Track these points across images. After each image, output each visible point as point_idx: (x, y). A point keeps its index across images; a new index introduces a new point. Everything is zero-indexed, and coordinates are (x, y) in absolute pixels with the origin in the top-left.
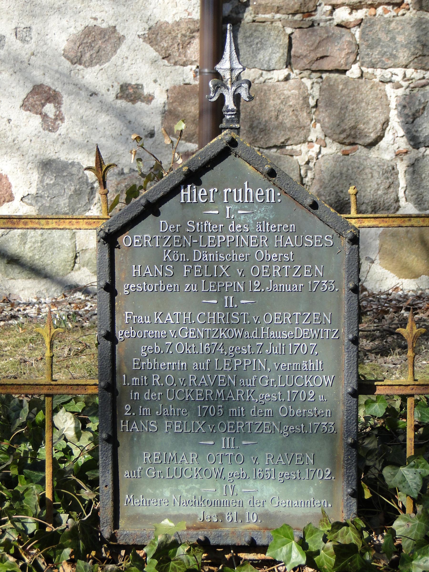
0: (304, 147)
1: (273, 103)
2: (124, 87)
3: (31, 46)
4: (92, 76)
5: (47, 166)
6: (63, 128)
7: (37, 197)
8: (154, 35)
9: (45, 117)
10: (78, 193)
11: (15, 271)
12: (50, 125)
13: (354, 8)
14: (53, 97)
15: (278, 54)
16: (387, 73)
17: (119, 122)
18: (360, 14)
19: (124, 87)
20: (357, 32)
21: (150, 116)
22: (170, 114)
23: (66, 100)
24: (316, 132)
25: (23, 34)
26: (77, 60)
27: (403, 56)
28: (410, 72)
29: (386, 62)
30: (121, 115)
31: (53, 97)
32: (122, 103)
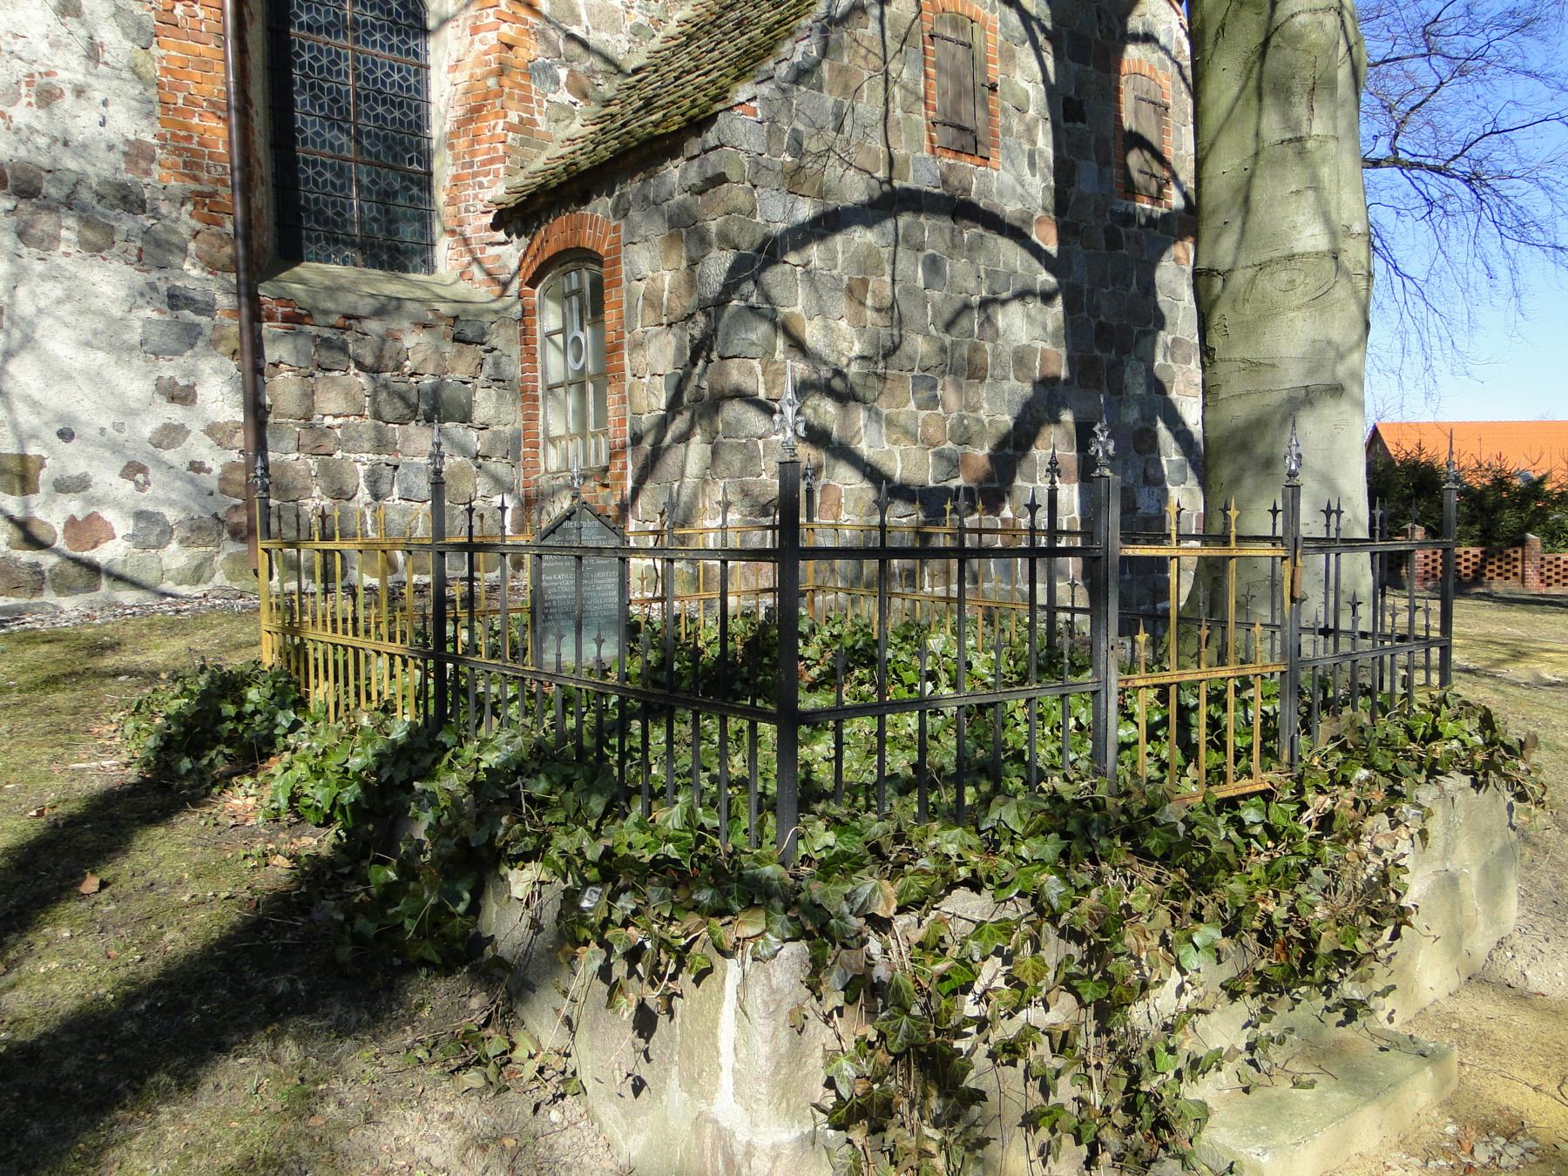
0: (309, 501)
1: (290, 474)
2: (192, 463)
3: (125, 435)
4: (169, 455)
5: (140, 515)
6: (149, 491)
7: (133, 536)
8: (211, 430)
9: (137, 483)
10: (163, 533)
11: (120, 585)
12: (141, 487)
13: (336, 416)
14: (143, 469)
15: (293, 444)
16: (357, 456)
17: (76, 473)
18: (340, 420)
19: (192, 463)
20: (338, 431)
21: (211, 481)
22: (223, 479)
23: (151, 471)
24: (317, 492)
25: (119, 427)
26: (158, 445)
27: (367, 446)
28: (371, 456)
29: (1325, 727)
30: (192, 481)
31: (143, 469)
32: (191, 473)
